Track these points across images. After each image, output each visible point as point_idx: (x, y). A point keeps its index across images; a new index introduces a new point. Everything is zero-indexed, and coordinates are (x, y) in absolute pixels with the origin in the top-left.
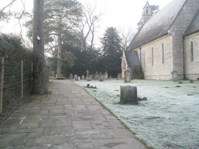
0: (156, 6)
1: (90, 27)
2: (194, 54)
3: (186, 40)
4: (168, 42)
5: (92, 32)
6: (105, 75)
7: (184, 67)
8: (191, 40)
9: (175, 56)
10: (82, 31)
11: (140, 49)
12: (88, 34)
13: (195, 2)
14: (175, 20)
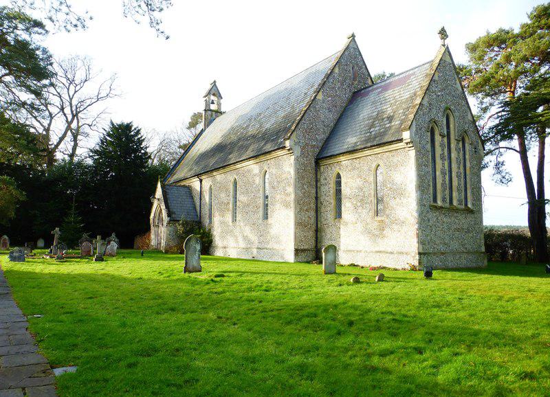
0: (190, 121)
1: (69, 123)
2: (344, 201)
3: (322, 168)
4: (285, 166)
5: (73, 134)
6: (109, 243)
7: (317, 231)
8: (336, 170)
9: (300, 204)
10: (47, 130)
11: (201, 181)
12: (61, 139)
13: (339, 88)
14: (301, 120)
